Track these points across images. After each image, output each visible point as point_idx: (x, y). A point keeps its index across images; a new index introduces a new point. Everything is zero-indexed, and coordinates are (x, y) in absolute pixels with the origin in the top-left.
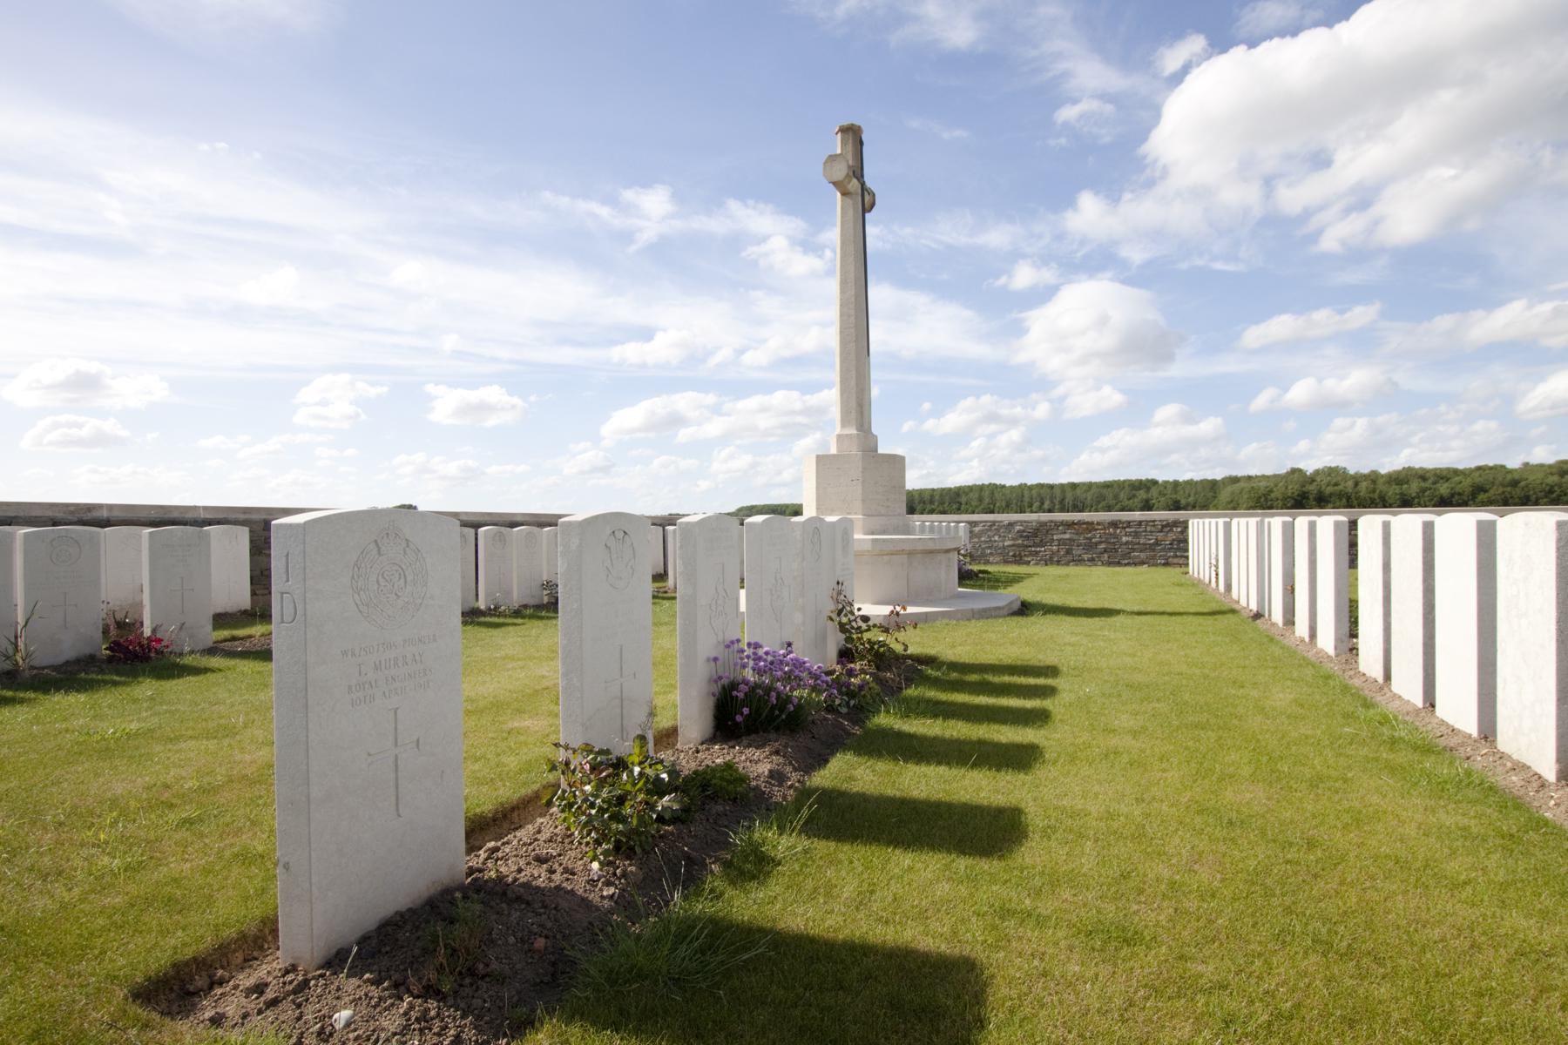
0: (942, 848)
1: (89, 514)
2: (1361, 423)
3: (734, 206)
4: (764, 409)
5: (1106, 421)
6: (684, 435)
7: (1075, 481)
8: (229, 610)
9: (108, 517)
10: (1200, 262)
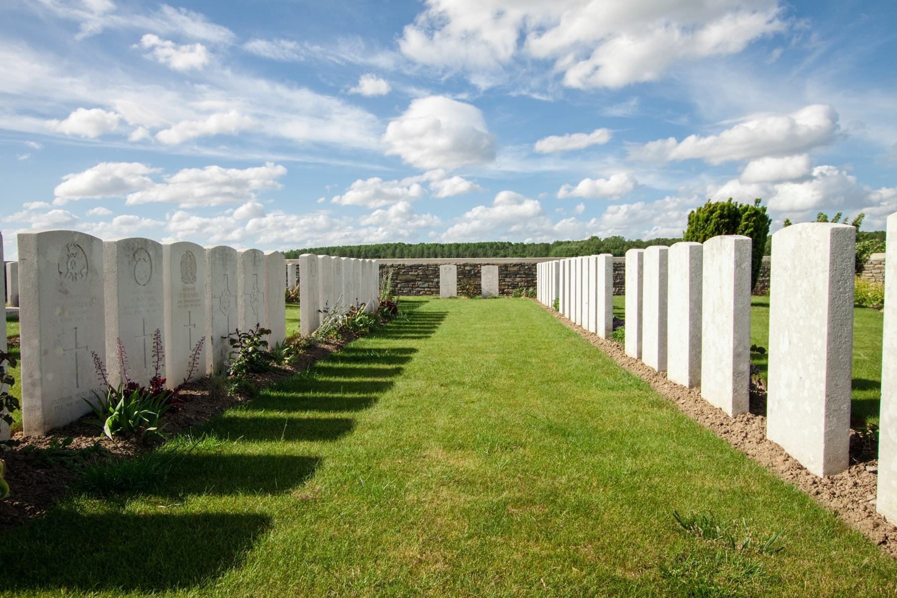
0: (258, 491)
2: (624, 208)
3: (168, 10)
4: (199, 180)
5: (462, 202)
6: (132, 199)
7: (459, 243)
10: (524, 93)
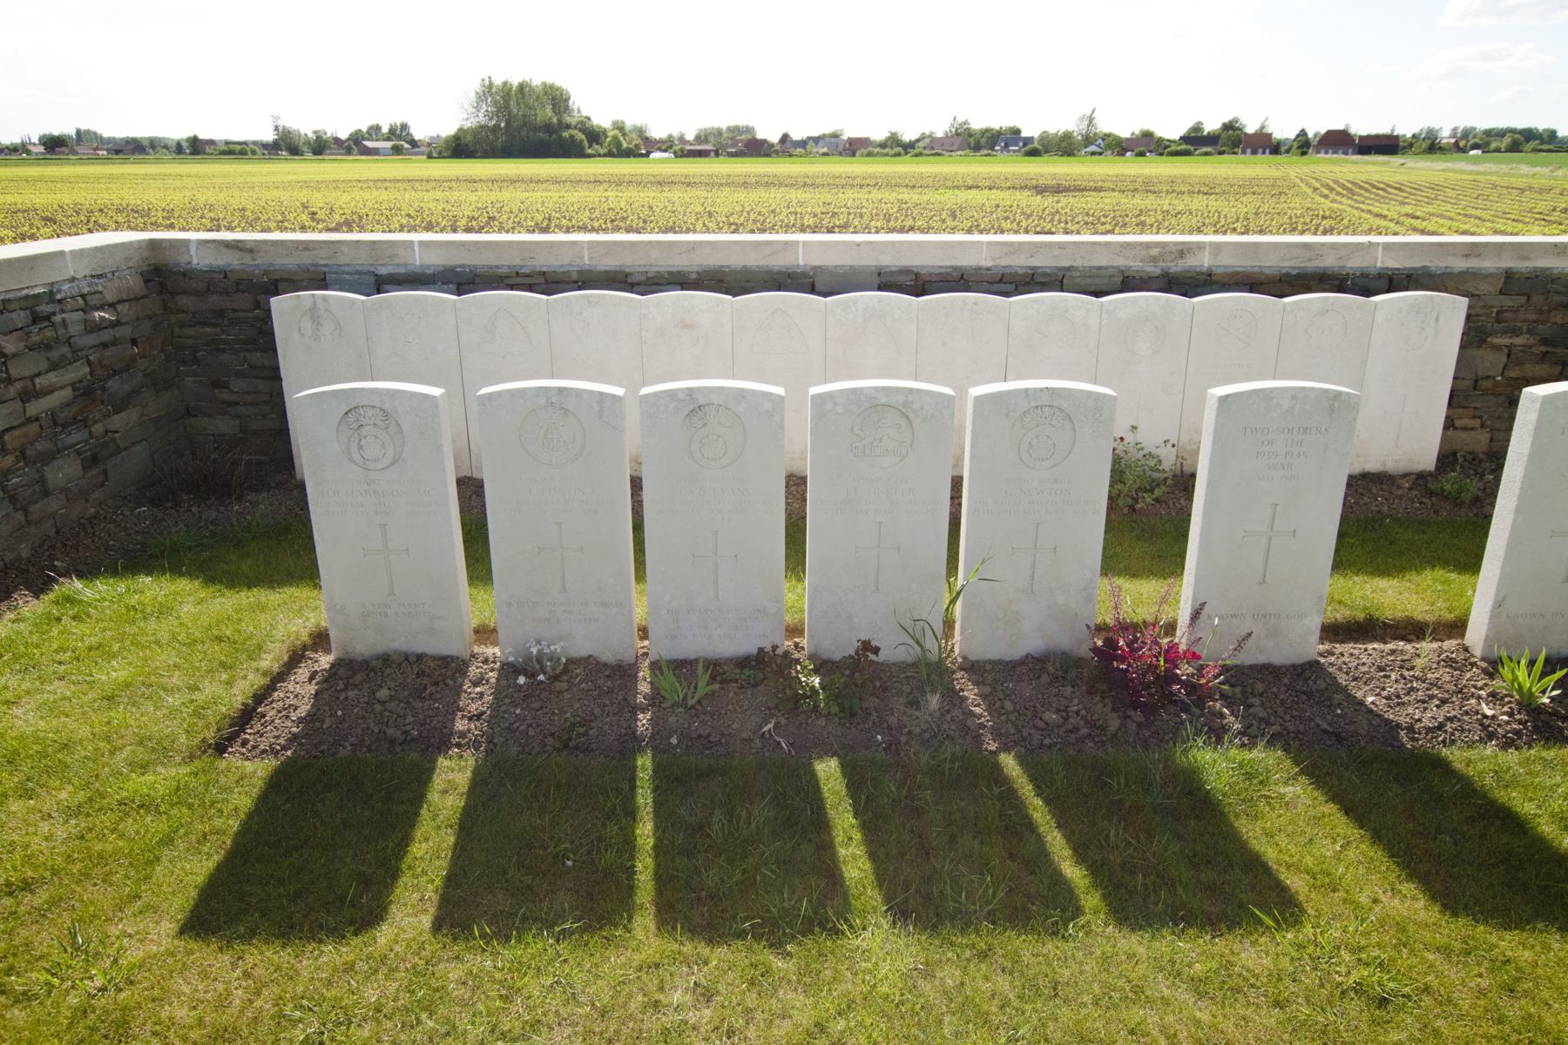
9: (1209, 268)
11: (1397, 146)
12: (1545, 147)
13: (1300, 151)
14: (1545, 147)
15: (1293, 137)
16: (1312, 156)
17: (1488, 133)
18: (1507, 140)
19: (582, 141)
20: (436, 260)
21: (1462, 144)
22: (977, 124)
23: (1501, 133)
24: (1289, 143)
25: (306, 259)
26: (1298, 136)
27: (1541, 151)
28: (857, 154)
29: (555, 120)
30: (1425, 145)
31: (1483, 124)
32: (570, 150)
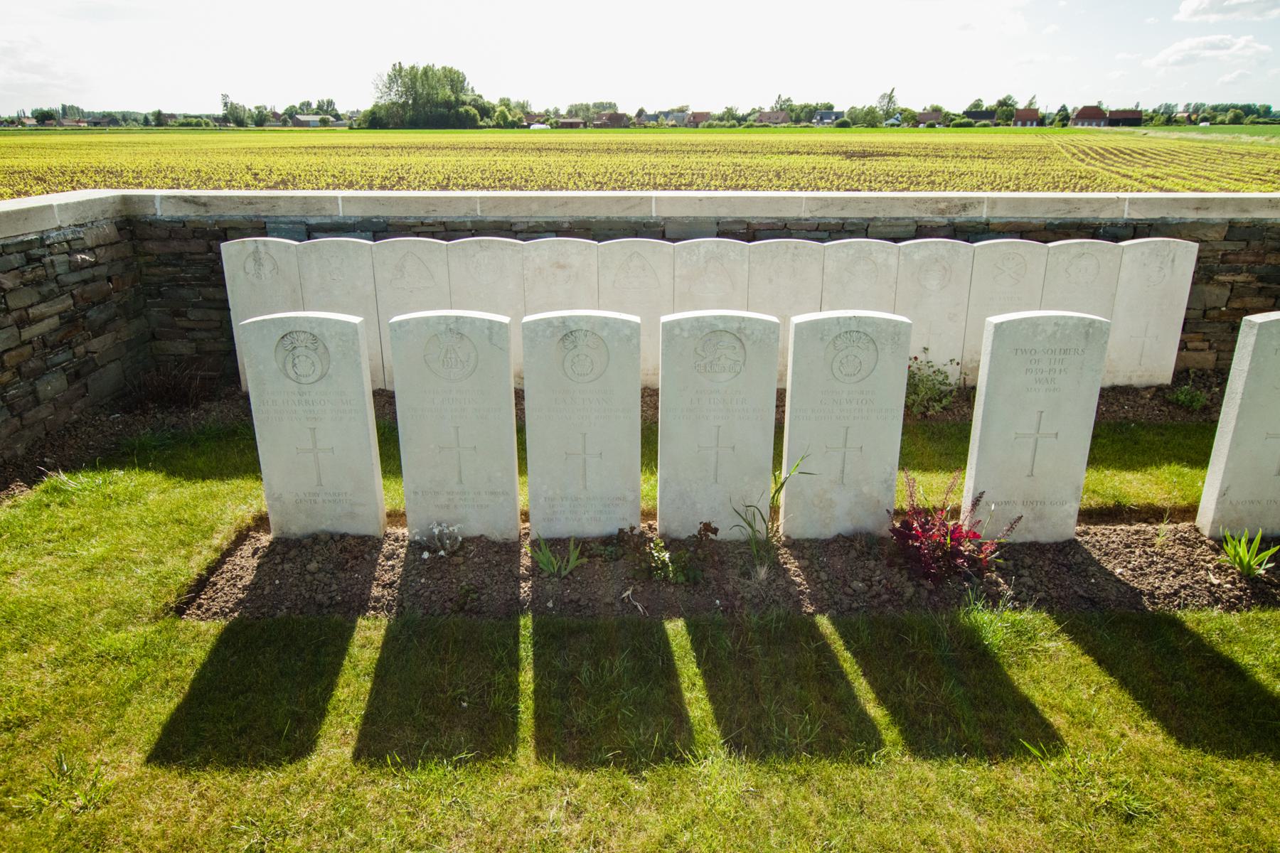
1: (963, 213)
8: (1136, 381)
9: (987, 219)
11: (1140, 119)
12: (1261, 120)
13: (1061, 123)
14: (1261, 120)
15: (1056, 112)
16: (1071, 127)
17: (1215, 109)
18: (1230, 114)
19: (475, 115)
20: (356, 213)
21: (1193, 117)
22: (798, 102)
23: (1225, 109)
24: (1052, 117)
25: (249, 211)
26: (1059, 111)
27: (1258, 123)
28: (700, 126)
29: (453, 98)
30: (1163, 118)
31: (1210, 101)
32: (465, 122)
